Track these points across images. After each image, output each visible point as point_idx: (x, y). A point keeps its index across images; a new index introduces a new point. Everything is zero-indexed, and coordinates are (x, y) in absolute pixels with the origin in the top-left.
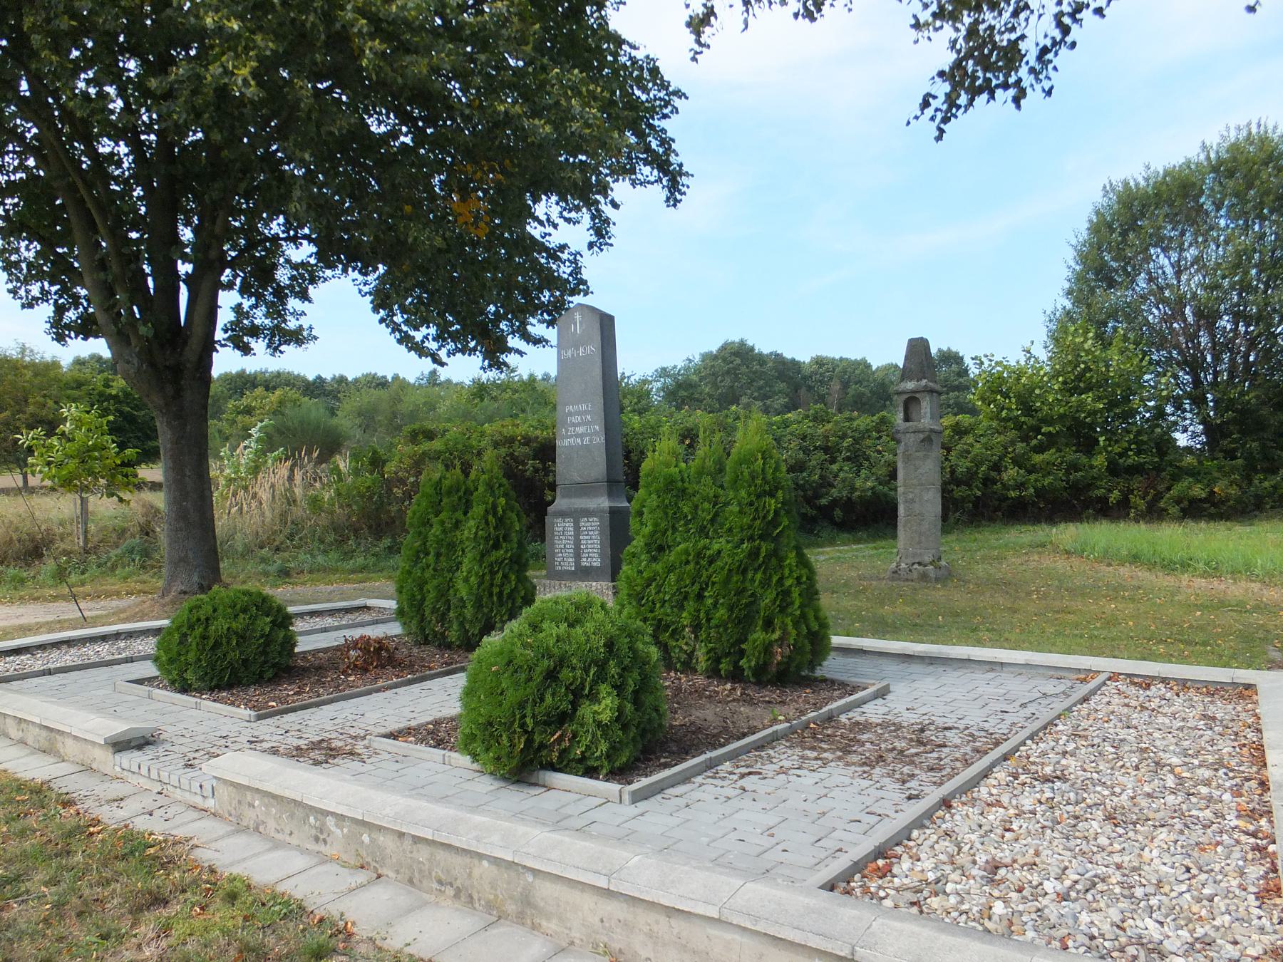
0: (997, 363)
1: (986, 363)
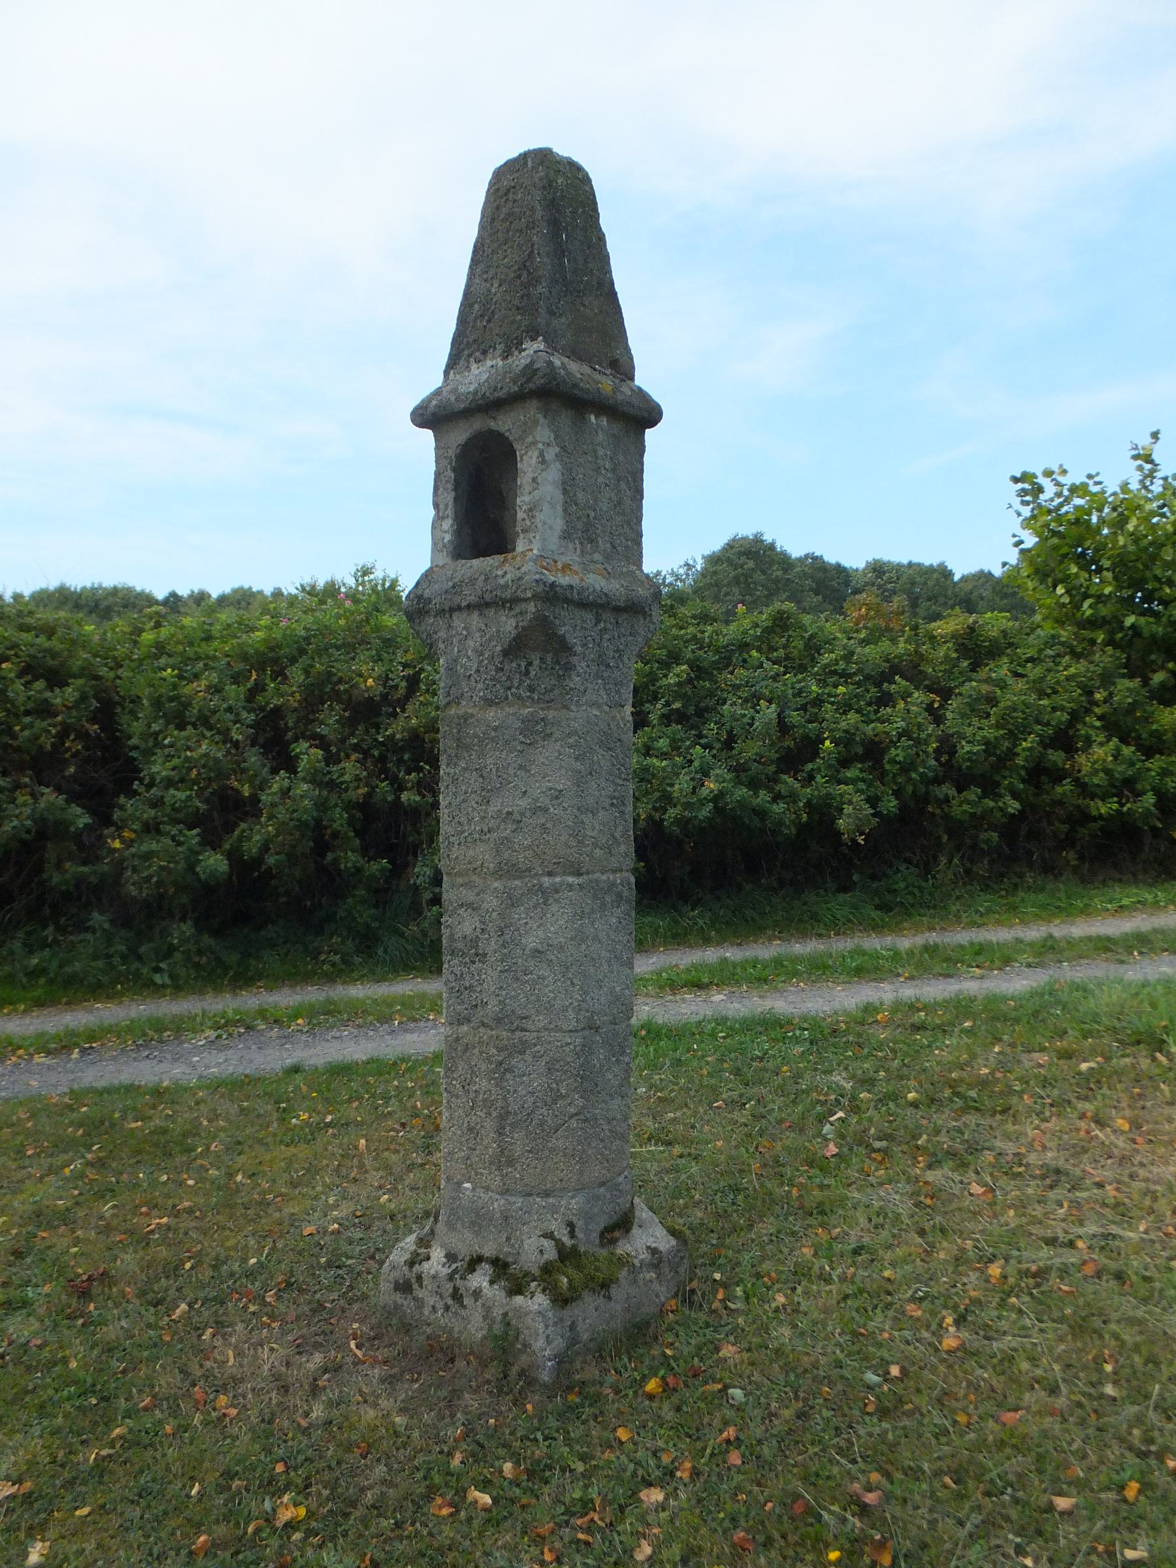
0: (1074, 489)
1: (1050, 490)
